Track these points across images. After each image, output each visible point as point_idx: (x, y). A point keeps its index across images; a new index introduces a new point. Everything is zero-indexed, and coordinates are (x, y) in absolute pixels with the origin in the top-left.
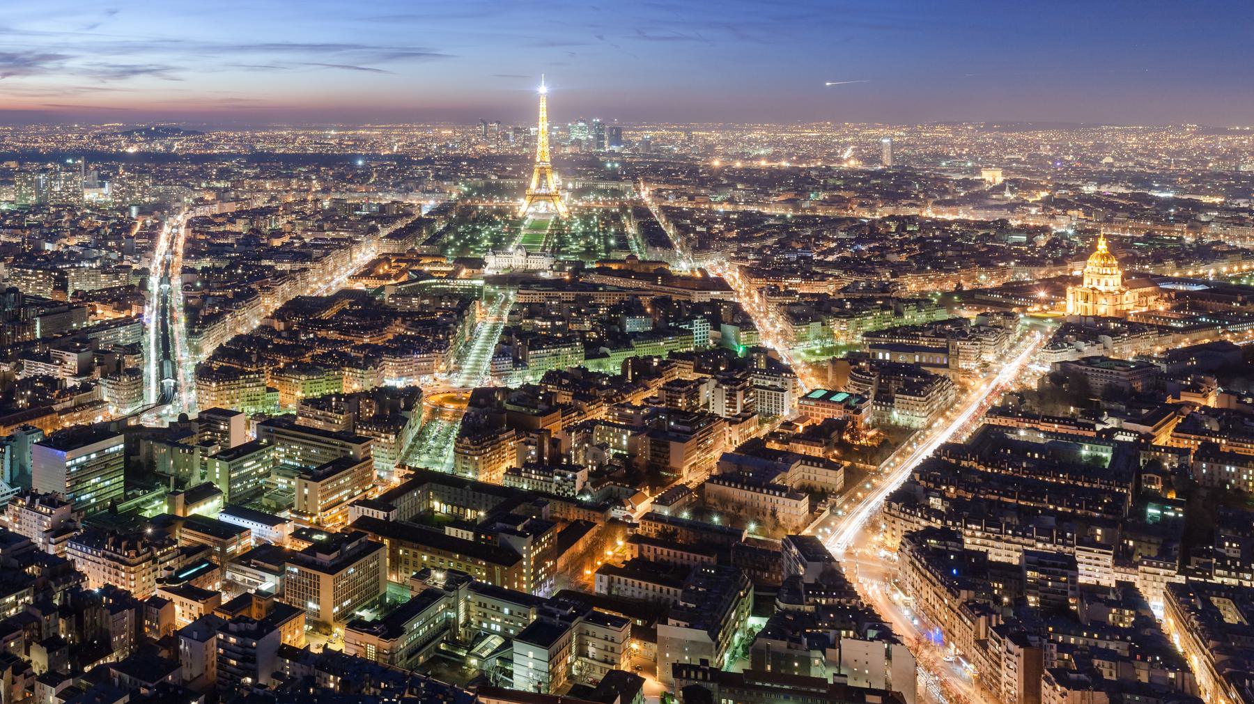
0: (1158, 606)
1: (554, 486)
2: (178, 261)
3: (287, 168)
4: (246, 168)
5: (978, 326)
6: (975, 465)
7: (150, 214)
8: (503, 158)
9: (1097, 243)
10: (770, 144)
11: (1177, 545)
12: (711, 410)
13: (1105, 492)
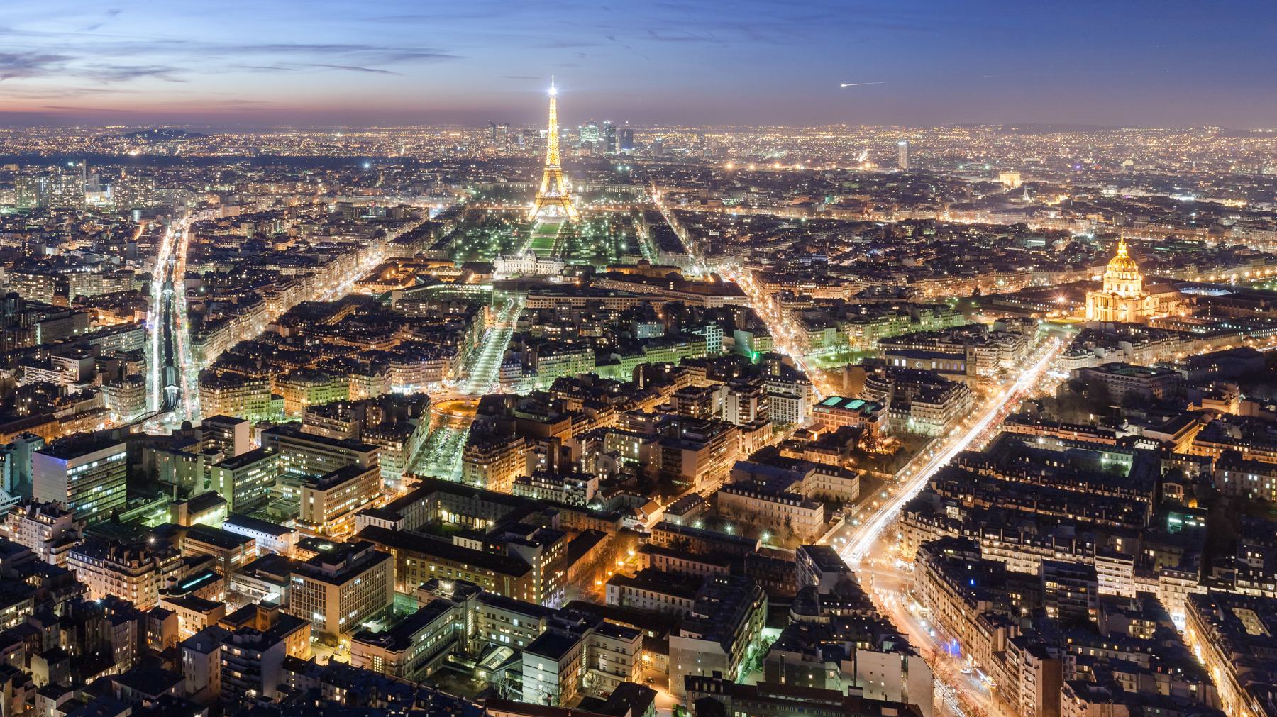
0: (1179, 617)
1: (564, 495)
2: (182, 265)
3: (292, 171)
4: (251, 171)
5: (995, 332)
6: (993, 473)
7: (153, 217)
8: (512, 161)
9: (1117, 247)
10: (784, 147)
11: (1198, 555)
12: (724, 418)
13: (1125, 501)
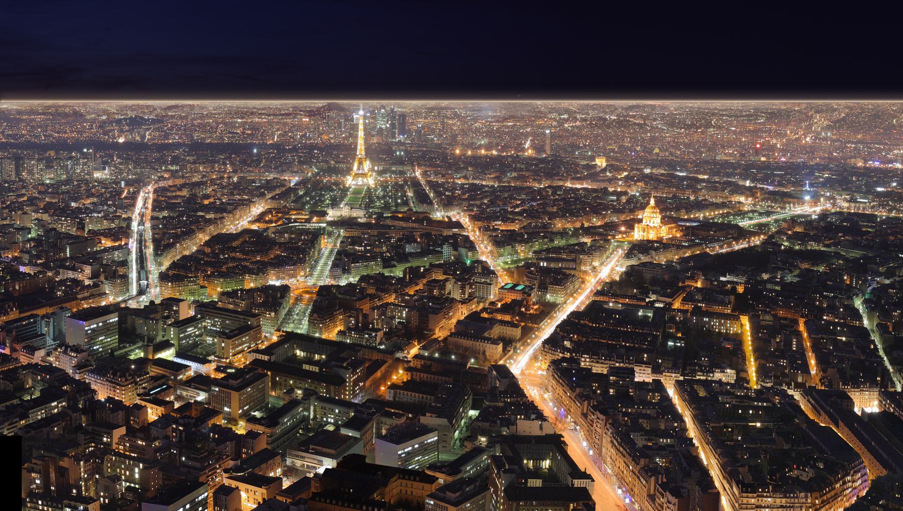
0: (671, 392)
1: (365, 341)
2: (149, 212)
4: (188, 155)
5: (591, 247)
7: (132, 185)
8: (337, 147)
9: (650, 200)
11: (681, 361)
12: (452, 296)
13: (649, 334)
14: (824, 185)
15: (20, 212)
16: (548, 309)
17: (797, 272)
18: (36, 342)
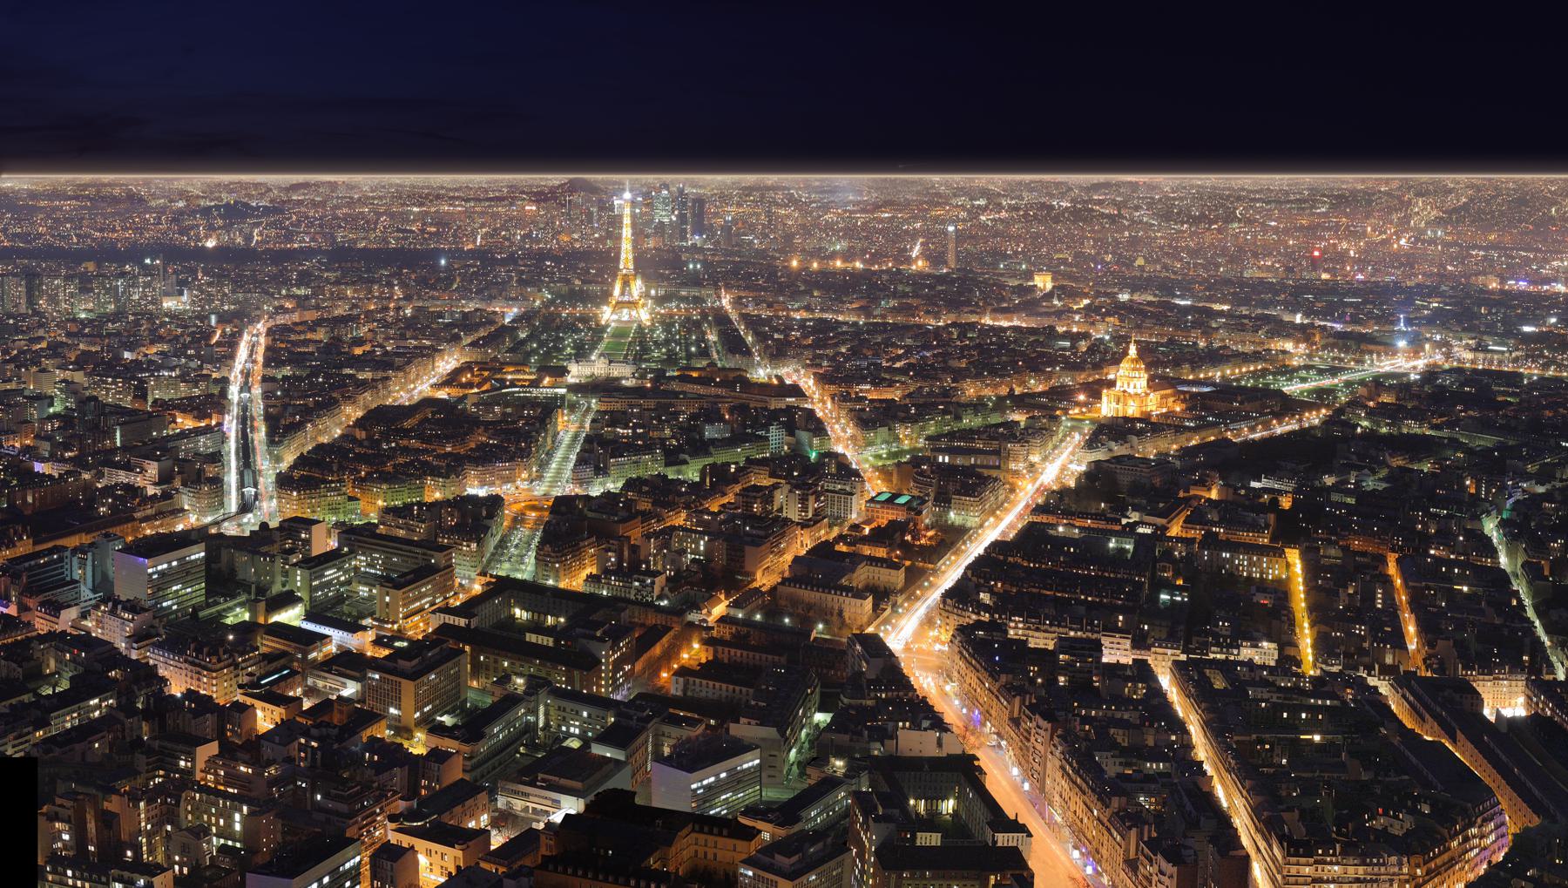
0: (1166, 681)
1: (633, 592)
2: (258, 369)
4: (327, 270)
5: (1026, 429)
7: (229, 322)
8: (586, 255)
9: (1128, 348)
11: (1182, 627)
12: (785, 515)
13: (1127, 581)
14: (1430, 321)
15: (34, 369)
16: (951, 537)
17: (1383, 473)
18: (62, 594)
